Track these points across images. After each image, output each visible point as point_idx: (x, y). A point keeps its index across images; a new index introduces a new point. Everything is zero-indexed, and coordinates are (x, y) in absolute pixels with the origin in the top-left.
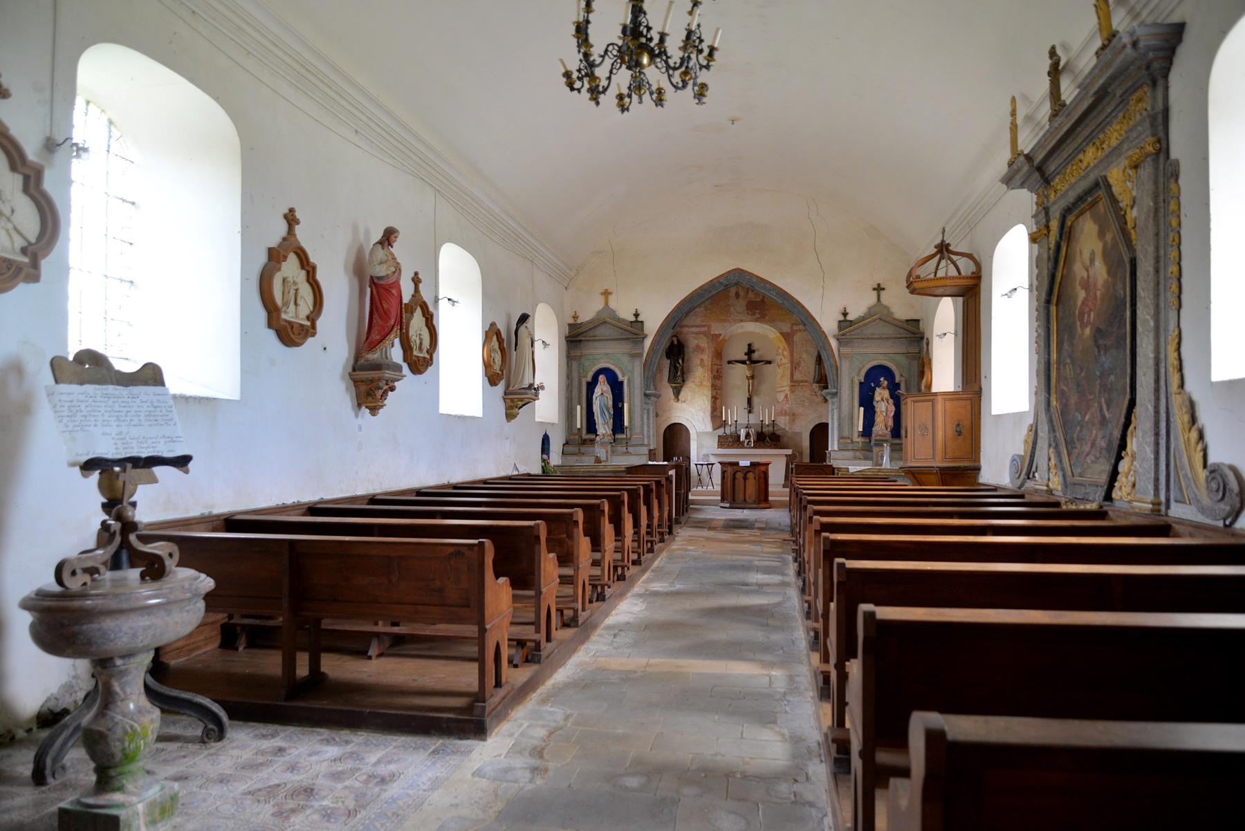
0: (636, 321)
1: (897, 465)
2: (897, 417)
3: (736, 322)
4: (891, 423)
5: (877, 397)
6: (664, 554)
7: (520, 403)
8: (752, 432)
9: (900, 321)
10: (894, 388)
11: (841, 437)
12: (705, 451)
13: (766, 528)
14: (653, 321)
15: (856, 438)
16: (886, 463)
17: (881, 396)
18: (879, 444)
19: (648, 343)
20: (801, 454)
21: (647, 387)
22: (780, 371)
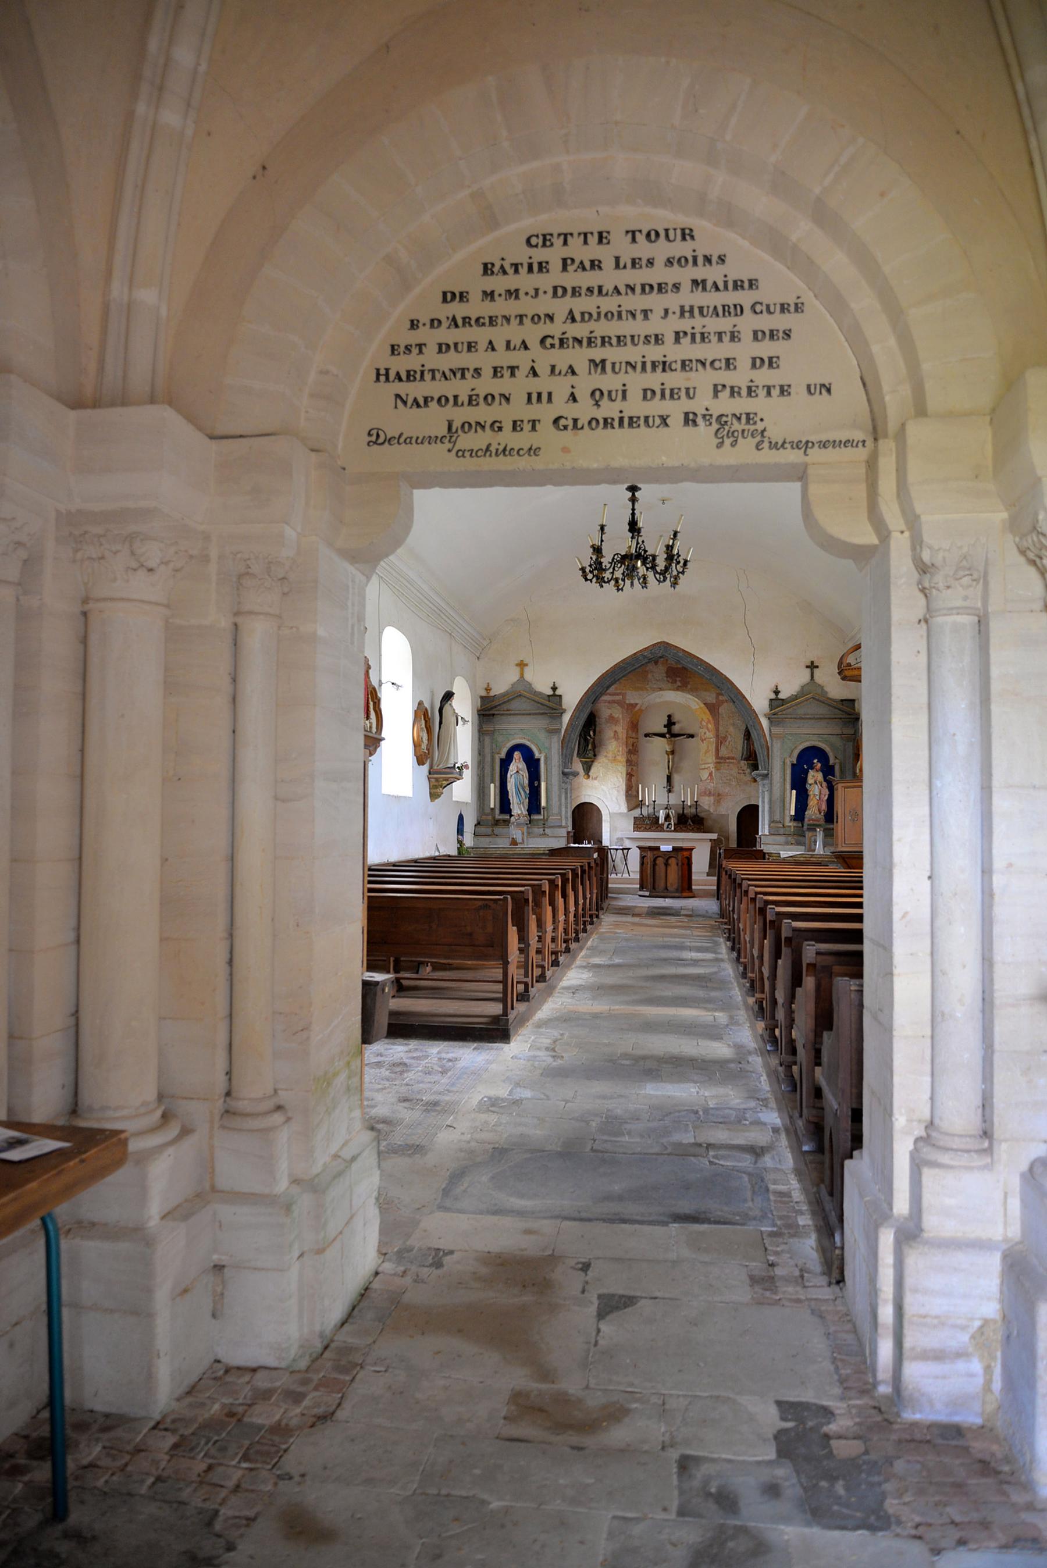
0: (554, 695)
1: (828, 852)
2: (831, 801)
3: (654, 690)
4: (824, 807)
5: (810, 780)
6: (594, 936)
7: (445, 783)
8: (672, 813)
9: (834, 700)
10: (828, 771)
11: (772, 821)
12: (619, 835)
13: (692, 915)
14: (572, 696)
15: (788, 822)
16: (819, 849)
17: (814, 777)
18: (812, 828)
19: (566, 718)
20: (727, 839)
21: (565, 765)
22: (704, 746)
